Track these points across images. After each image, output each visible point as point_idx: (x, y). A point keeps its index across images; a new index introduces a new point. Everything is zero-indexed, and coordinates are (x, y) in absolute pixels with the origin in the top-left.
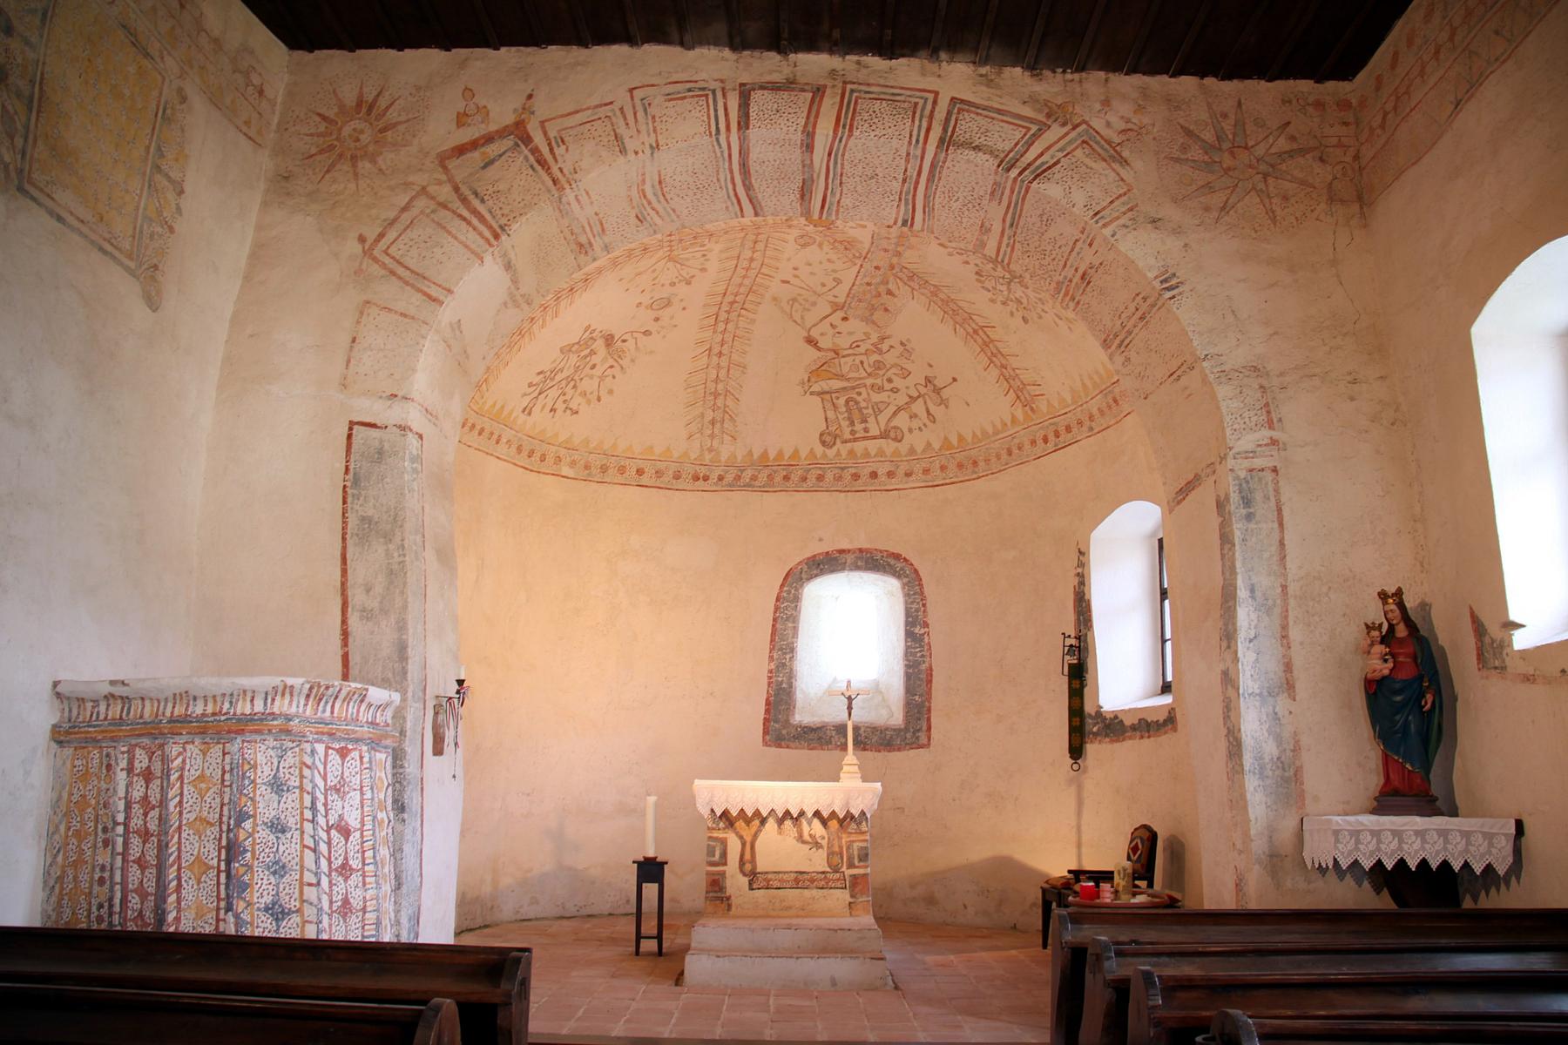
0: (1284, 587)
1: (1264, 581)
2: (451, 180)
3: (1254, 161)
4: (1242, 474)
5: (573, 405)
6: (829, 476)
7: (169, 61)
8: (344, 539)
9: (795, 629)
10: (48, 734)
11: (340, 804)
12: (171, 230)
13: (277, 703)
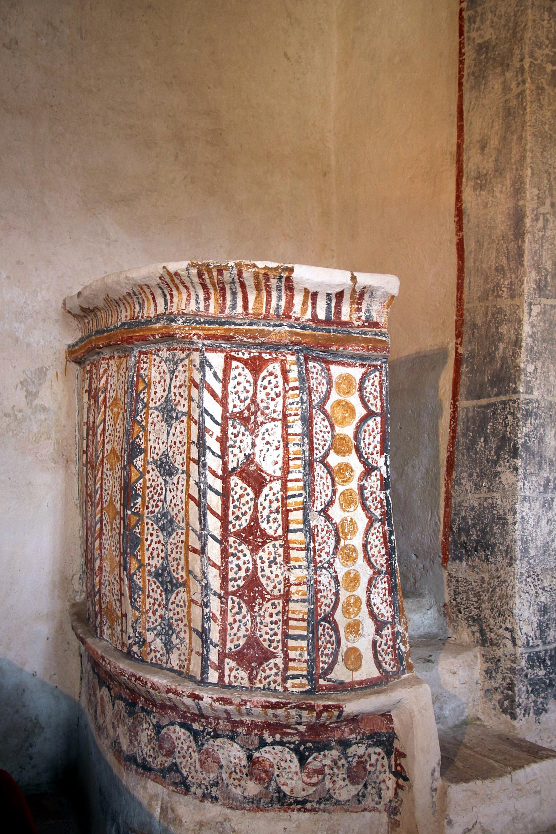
8: (460, 85)
10: (63, 354)
11: (248, 440)
13: (175, 299)
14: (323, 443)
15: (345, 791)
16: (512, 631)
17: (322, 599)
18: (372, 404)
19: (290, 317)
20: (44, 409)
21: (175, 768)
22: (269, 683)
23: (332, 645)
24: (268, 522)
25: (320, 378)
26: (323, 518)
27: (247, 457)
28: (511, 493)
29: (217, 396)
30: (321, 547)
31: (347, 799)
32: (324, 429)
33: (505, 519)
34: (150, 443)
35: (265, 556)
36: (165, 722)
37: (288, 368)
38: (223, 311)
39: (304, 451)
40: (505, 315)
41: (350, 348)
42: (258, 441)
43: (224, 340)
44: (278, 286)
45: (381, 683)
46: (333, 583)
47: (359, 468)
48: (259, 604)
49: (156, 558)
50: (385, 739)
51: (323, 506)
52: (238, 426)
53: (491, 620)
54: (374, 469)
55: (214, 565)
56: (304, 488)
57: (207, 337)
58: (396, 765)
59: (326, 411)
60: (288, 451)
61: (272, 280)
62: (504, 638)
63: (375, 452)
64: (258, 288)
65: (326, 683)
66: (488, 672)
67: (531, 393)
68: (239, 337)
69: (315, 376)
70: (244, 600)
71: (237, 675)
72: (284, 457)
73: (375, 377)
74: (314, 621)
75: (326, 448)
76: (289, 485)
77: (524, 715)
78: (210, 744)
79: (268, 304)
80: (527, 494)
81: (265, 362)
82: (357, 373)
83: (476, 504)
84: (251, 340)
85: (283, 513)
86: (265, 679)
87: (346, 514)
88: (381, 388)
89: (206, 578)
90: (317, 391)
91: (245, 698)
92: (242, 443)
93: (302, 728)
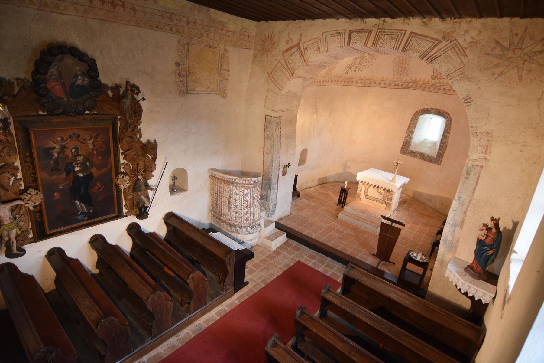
0: (470, 201)
1: (465, 197)
2: (284, 59)
3: (522, 55)
4: (470, 166)
5: (361, 69)
6: (432, 88)
7: (220, 45)
9: (415, 127)
12: (228, 80)
71: (245, 222)
92: (246, 198)
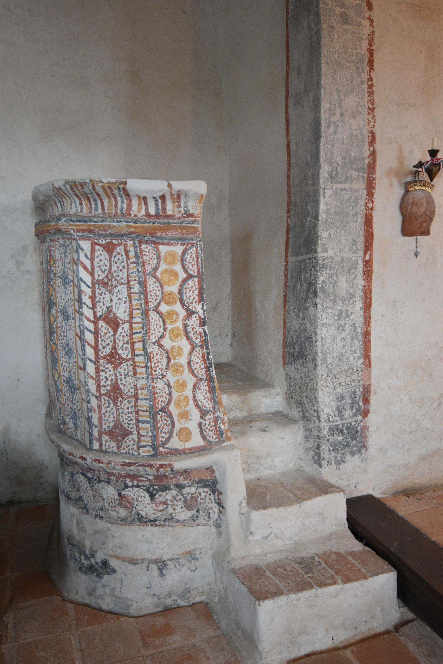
8: (287, 25)
11: (108, 297)
13: (65, 205)
14: (156, 298)
15: (185, 515)
16: (317, 412)
17: (159, 398)
18: (191, 270)
19: (130, 214)
20: (29, 272)
21: (80, 499)
22: (129, 450)
23: (168, 426)
24: (123, 350)
25: (151, 255)
26: (157, 347)
27: (108, 308)
28: (314, 321)
29: (88, 269)
30: (156, 365)
31: (185, 519)
32: (156, 289)
33: (311, 338)
34: (58, 299)
35: (122, 371)
36: (75, 472)
37: (128, 250)
38: (91, 212)
39: (141, 304)
40: (310, 197)
41: (170, 234)
42: (114, 298)
43: (88, 232)
44: (119, 194)
45: (206, 449)
46: (166, 387)
47: (182, 313)
48: (120, 401)
49: (66, 372)
50: (210, 483)
51: (157, 339)
52: (101, 288)
53: (307, 404)
54: (193, 313)
55: (91, 377)
56: (142, 328)
57: (79, 231)
58: (219, 499)
59: (157, 276)
60: (132, 304)
61: (114, 190)
62: (314, 416)
63: (194, 302)
64: (107, 195)
65: (164, 450)
66: (306, 438)
67: (327, 252)
68: (96, 230)
69: (147, 253)
70: (111, 399)
72: (130, 308)
73: (193, 251)
74: (153, 412)
75: (158, 301)
76: (134, 326)
77: (327, 465)
78: (98, 486)
79: (116, 206)
80: (325, 321)
81: (115, 246)
82: (179, 249)
83: (297, 328)
84: (103, 232)
85: (131, 344)
86: (127, 447)
87: (174, 343)
88: (197, 259)
89: (87, 385)
90: (149, 264)
91: (111, 459)
93: (151, 477)
